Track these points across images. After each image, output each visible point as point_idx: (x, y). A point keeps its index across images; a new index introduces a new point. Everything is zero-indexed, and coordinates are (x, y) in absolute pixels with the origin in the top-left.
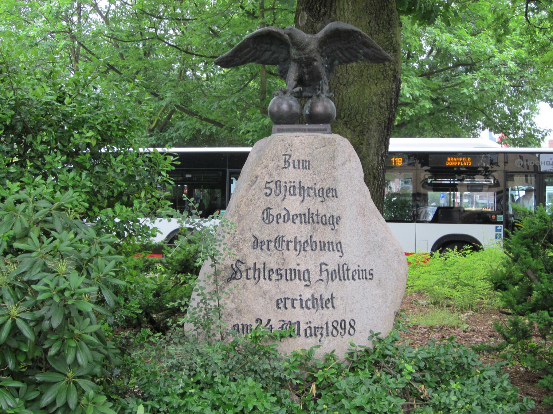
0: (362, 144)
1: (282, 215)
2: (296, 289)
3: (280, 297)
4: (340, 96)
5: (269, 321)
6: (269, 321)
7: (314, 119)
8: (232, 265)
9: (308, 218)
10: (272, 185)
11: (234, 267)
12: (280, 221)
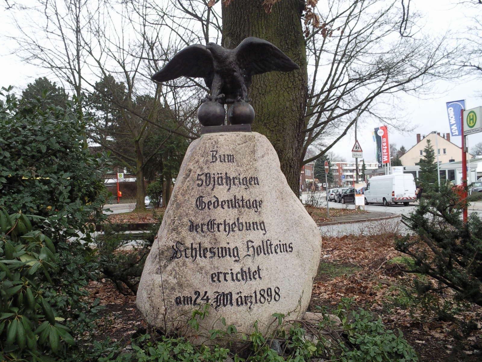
0: (279, 141)
1: (212, 202)
2: (228, 264)
5: (206, 292)
8: (173, 246)
9: (234, 203)
10: (203, 177)
11: (175, 247)
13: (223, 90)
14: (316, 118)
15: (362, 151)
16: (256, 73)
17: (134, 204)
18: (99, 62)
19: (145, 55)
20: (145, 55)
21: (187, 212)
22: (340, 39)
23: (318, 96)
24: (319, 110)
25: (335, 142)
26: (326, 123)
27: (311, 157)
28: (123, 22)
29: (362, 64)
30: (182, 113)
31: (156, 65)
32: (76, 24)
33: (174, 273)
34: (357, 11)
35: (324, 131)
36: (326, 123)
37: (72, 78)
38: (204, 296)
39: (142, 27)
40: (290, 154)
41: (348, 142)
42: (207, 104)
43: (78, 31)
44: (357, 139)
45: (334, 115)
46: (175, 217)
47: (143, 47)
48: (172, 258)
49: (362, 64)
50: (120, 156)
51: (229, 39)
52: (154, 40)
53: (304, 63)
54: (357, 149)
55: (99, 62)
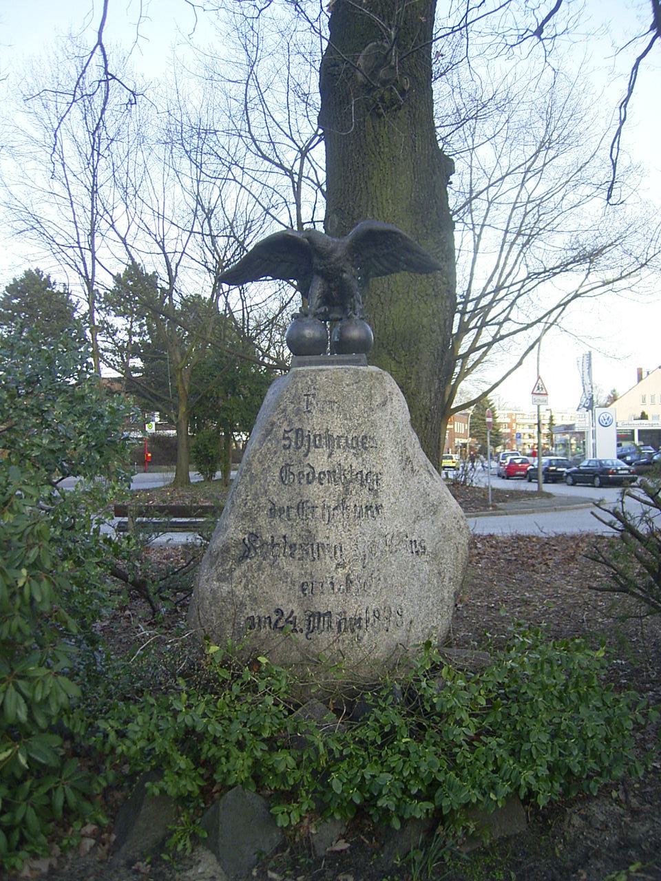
0: (410, 378)
1: (305, 473)
3: (306, 580)
4: (382, 318)
5: (292, 612)
6: (292, 612)
7: (344, 348)
8: (244, 539)
10: (292, 435)
11: (247, 541)
12: (304, 481)
13: (326, 299)
14: (474, 336)
15: (546, 394)
16: (378, 275)
17: (172, 475)
18: (124, 240)
19: (197, 228)
20: (197, 228)
21: (266, 488)
22: (514, 208)
23: (478, 299)
24: (478, 324)
25: (504, 378)
26: (489, 345)
27: (464, 401)
28: (166, 176)
29: (549, 249)
30: (252, 324)
31: (214, 244)
32: (91, 179)
33: (244, 581)
34: (539, 163)
35: (486, 358)
36: (489, 345)
37: (81, 266)
38: (290, 617)
39: (195, 184)
40: (426, 399)
41: (522, 382)
42: (301, 321)
43: (94, 192)
44: (540, 374)
45: (503, 332)
46: (248, 496)
47: (196, 215)
48: (244, 557)
49: (549, 249)
50: (148, 391)
51: (336, 219)
52: (213, 202)
53: (448, 255)
54: (539, 391)
55: (124, 240)
